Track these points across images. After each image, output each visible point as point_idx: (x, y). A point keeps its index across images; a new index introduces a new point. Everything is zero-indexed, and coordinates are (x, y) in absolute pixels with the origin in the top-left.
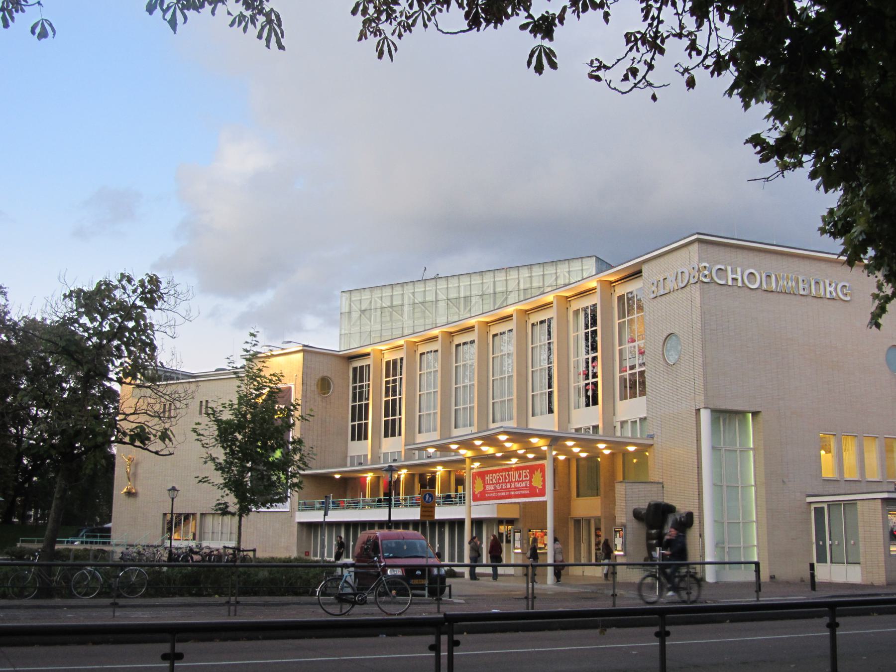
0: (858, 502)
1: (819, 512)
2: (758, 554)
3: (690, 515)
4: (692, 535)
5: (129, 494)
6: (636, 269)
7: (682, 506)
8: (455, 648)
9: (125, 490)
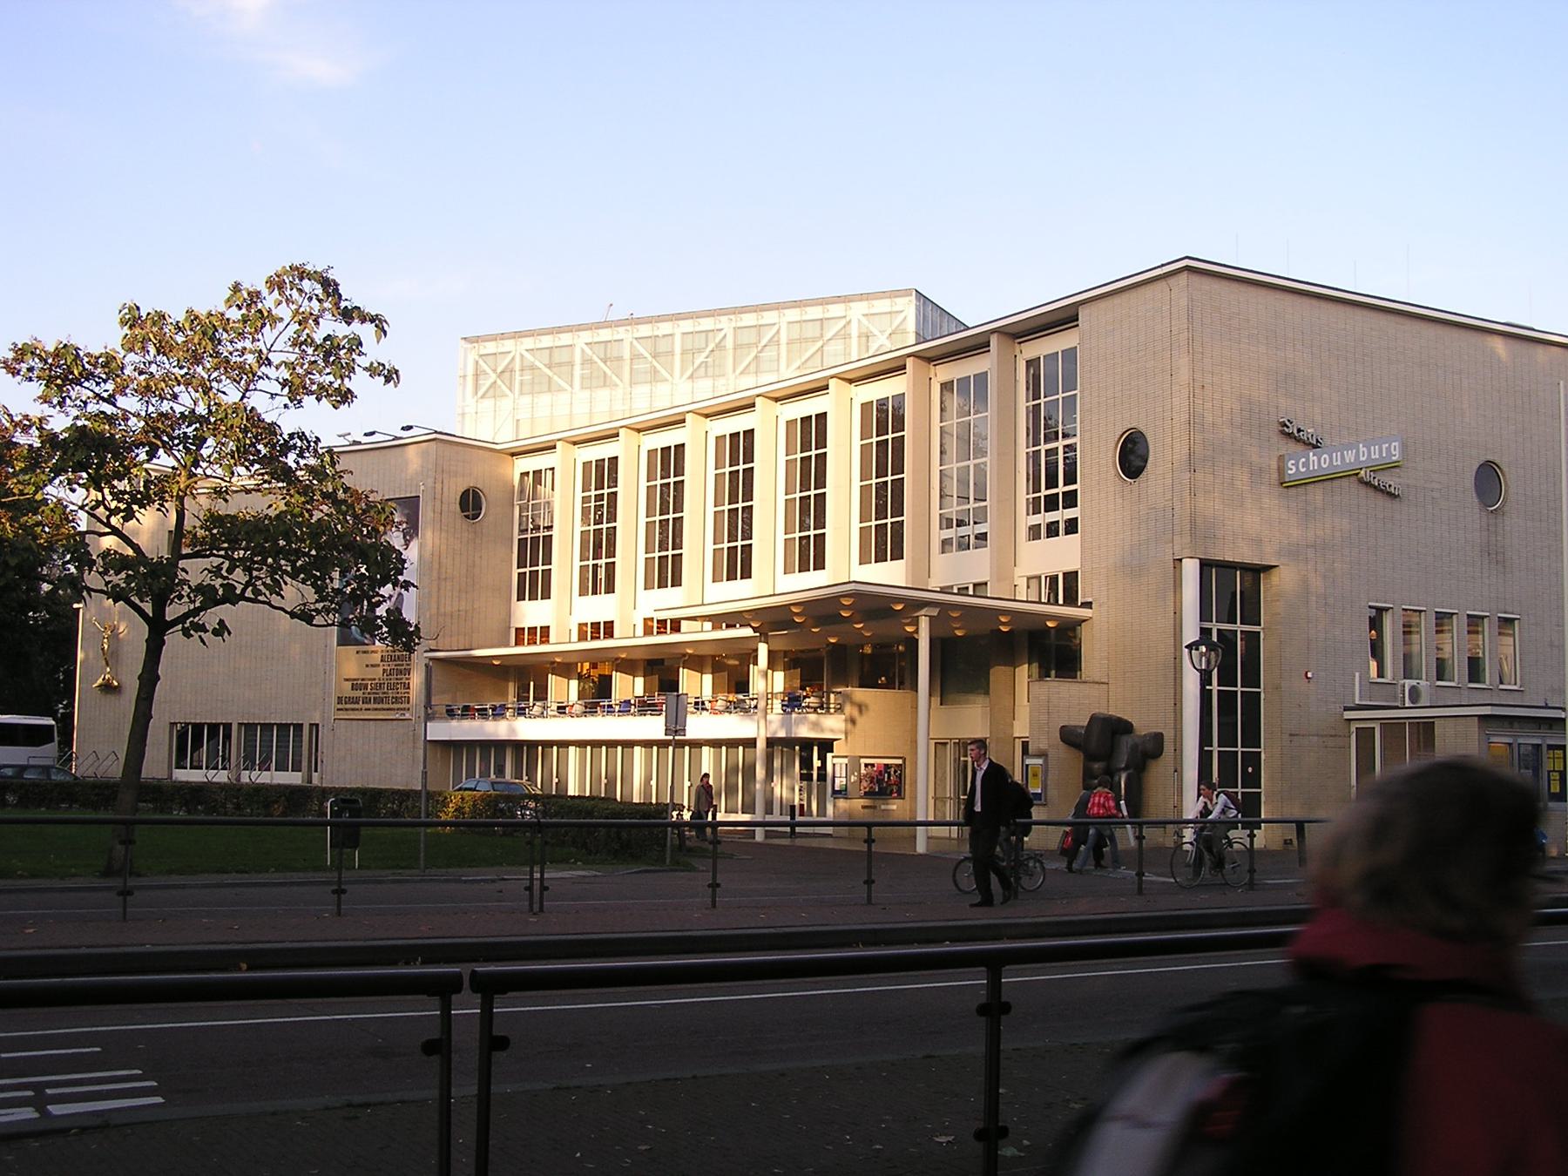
0: (1437, 721)
1: (1365, 736)
2: (101, 1125)
3: (1158, 738)
4: (1158, 771)
5: (107, 688)
6: (982, 340)
7: (1143, 724)
8: (436, 1035)
9: (100, 681)
